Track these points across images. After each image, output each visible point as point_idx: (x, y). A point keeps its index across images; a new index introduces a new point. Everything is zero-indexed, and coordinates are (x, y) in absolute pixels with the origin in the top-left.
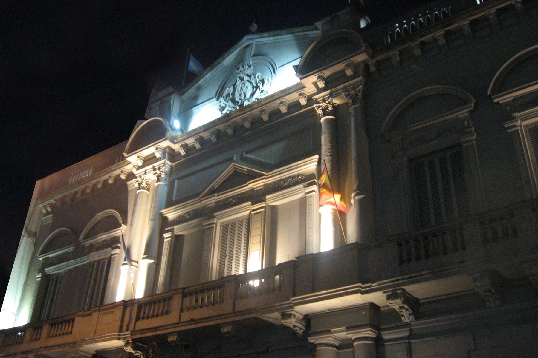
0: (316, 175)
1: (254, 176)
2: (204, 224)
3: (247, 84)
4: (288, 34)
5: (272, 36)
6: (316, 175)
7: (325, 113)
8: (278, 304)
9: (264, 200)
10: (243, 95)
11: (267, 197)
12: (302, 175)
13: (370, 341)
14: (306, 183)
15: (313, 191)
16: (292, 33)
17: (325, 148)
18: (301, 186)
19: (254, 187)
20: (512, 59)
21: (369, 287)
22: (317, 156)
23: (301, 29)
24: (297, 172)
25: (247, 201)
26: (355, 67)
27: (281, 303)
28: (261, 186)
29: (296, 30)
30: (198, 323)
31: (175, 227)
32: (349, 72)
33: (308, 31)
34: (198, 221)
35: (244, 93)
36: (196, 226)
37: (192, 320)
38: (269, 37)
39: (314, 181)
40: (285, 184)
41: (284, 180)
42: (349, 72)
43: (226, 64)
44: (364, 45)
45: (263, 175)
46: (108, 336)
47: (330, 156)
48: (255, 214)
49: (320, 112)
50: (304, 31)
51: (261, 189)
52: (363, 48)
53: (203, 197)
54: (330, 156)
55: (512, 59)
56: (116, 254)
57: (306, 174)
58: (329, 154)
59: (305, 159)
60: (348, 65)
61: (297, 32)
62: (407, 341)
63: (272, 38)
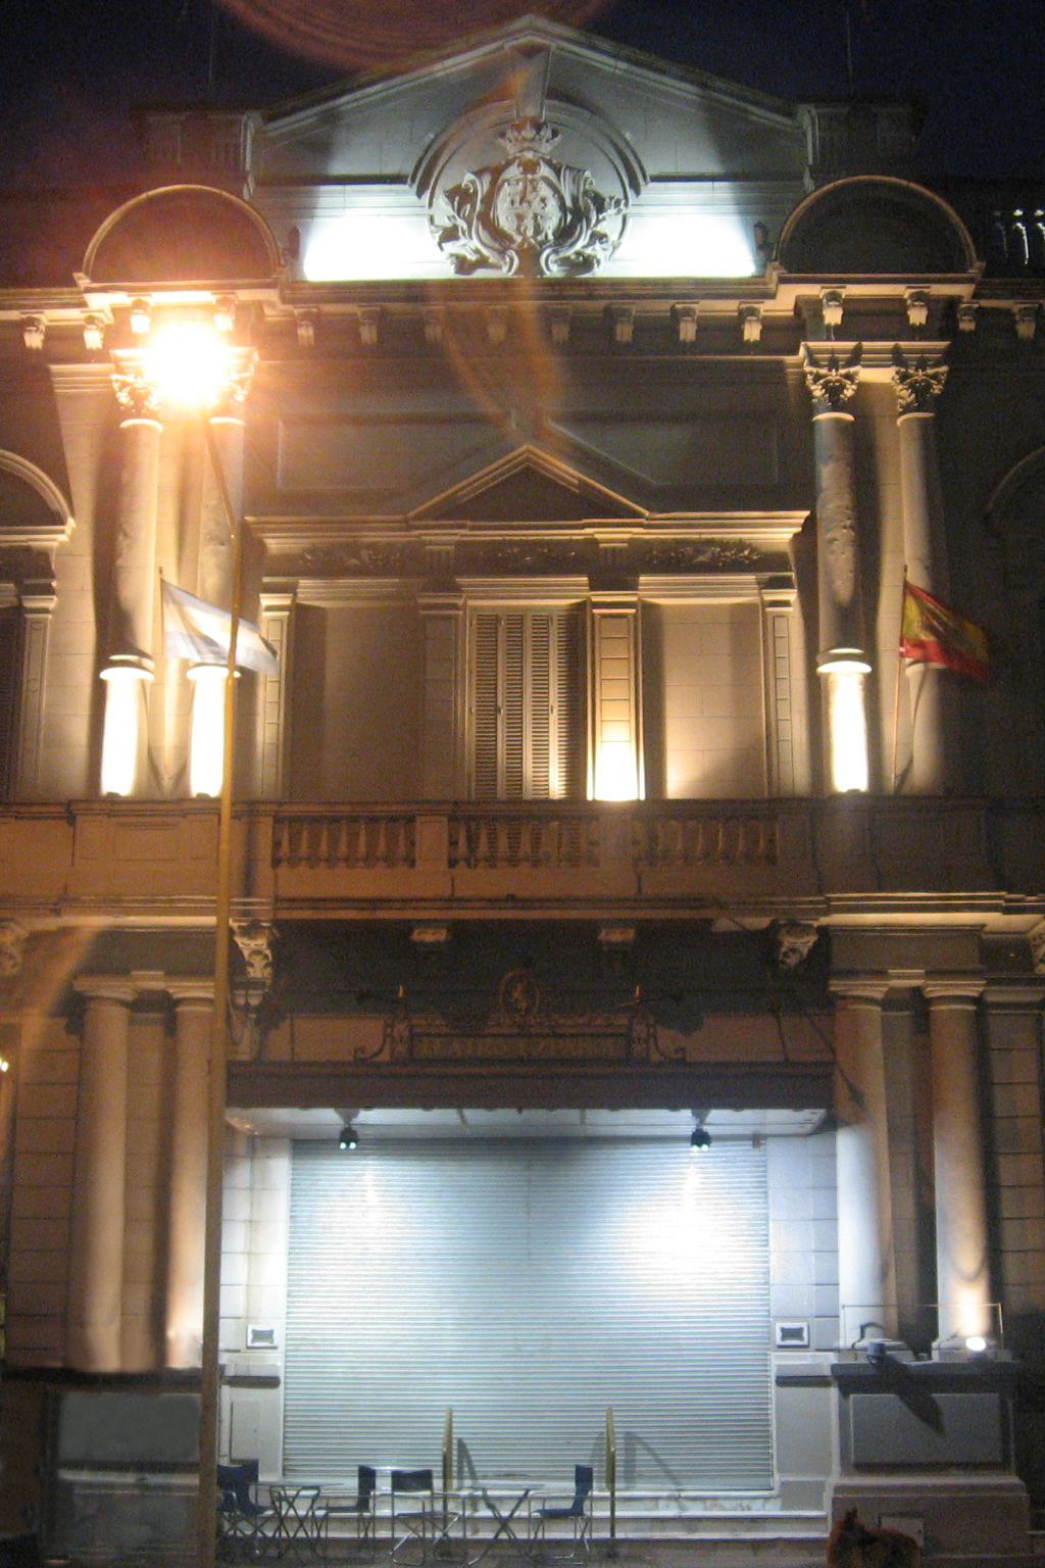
0: (791, 558)
1: (607, 510)
2: (422, 601)
3: (544, 190)
4: (682, 79)
5: (628, 60)
6: (791, 558)
7: (836, 404)
8: (785, 899)
9: (633, 586)
10: (529, 223)
11: (643, 579)
12: (753, 550)
13: (968, 1004)
14: (768, 575)
15: (786, 604)
16: (703, 86)
17: (837, 502)
18: (751, 578)
19: (597, 536)
20: (862, 178)
21: (1018, 901)
22: (806, 513)
23: (735, 87)
24: (739, 536)
25: (580, 573)
26: (945, 314)
27: (795, 899)
28: (622, 541)
29: (719, 83)
30: (523, 908)
31: (303, 582)
32: (918, 316)
33: (756, 103)
34: (393, 585)
35: (535, 216)
36: (389, 597)
37: (511, 898)
38: (616, 57)
39: (790, 578)
40: (701, 558)
41: (701, 546)
42: (918, 316)
43: (439, 75)
44: (978, 264)
45: (640, 516)
46: (179, 901)
47: (852, 527)
48: (604, 616)
49: (818, 391)
50: (743, 99)
51: (621, 550)
52: (972, 272)
53: (418, 517)
54: (852, 527)
55: (862, 178)
56: (46, 611)
57: (763, 550)
58: (848, 522)
59: (772, 510)
60: (918, 297)
61: (719, 91)
62: (1036, 1012)
63: (623, 65)
